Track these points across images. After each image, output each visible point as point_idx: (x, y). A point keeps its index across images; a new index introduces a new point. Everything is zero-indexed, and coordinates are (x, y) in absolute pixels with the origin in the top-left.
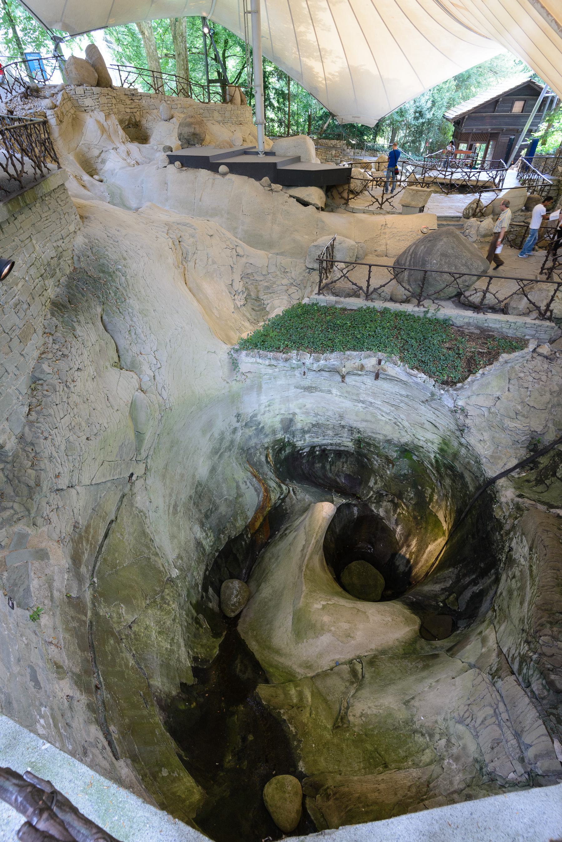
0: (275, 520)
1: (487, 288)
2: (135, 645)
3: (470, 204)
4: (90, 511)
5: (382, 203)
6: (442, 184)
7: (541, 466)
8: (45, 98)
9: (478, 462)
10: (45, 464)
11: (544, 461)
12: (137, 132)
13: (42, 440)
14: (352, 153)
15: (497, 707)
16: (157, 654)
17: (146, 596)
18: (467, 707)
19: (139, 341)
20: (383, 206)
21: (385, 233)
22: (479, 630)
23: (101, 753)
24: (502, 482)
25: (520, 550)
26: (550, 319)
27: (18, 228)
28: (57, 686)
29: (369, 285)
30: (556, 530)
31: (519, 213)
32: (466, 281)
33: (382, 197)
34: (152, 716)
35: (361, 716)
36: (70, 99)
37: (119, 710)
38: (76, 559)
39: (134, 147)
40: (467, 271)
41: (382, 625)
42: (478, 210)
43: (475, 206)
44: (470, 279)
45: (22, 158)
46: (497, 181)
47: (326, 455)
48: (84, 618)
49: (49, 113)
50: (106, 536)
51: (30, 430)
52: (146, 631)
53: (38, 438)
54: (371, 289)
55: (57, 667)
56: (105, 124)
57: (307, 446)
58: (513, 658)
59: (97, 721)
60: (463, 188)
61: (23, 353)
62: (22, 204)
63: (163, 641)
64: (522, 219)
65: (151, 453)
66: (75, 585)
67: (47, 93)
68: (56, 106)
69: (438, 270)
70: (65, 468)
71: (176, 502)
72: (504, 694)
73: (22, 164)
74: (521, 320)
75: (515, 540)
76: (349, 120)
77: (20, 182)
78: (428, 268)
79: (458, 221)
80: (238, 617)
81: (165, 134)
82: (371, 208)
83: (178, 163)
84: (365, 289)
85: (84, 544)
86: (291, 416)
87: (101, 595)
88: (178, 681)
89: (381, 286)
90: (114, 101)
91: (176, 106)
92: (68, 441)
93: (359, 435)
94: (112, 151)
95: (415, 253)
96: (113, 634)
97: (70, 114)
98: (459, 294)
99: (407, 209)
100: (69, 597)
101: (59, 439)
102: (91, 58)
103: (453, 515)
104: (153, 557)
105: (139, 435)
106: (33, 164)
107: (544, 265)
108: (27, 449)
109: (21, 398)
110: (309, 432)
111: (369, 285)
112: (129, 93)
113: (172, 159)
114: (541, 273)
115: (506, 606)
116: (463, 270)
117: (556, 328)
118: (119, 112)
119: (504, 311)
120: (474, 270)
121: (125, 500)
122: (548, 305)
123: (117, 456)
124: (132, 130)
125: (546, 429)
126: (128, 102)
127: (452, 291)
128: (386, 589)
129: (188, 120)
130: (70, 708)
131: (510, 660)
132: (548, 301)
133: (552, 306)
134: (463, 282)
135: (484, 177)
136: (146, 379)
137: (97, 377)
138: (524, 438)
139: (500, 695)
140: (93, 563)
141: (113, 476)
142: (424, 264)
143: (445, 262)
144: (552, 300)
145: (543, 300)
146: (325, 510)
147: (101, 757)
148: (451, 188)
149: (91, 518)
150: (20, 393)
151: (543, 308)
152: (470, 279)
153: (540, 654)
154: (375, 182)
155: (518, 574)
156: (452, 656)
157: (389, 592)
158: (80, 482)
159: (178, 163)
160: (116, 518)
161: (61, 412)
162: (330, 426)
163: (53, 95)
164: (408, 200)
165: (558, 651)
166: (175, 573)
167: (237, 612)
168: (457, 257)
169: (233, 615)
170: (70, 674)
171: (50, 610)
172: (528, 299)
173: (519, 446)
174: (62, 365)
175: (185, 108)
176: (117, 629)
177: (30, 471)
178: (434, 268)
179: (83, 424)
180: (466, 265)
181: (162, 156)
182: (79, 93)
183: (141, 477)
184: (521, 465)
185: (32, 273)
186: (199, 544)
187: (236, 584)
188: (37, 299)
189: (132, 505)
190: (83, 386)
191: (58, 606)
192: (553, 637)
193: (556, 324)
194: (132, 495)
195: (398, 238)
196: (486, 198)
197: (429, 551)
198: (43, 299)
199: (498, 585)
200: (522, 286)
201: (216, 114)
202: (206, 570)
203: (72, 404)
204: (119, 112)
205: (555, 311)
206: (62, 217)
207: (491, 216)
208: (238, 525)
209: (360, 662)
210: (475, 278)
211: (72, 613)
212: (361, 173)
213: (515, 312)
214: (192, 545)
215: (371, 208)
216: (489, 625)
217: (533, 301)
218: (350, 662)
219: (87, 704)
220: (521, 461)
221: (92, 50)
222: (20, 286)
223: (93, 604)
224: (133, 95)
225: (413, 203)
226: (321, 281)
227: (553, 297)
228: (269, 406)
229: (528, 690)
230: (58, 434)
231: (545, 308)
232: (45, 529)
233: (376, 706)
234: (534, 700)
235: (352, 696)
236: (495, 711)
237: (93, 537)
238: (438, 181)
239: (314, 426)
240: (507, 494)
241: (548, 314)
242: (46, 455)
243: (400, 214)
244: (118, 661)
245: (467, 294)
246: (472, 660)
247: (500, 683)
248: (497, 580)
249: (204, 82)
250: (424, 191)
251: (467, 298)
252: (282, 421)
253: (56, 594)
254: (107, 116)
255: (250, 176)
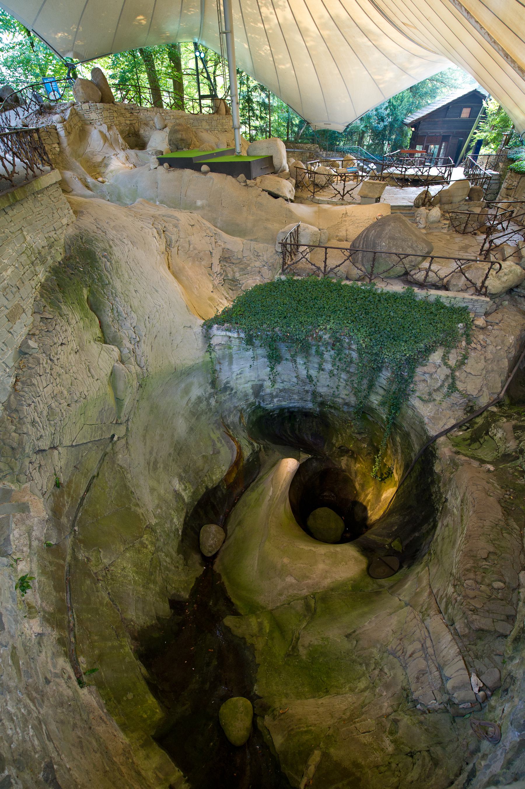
0: (247, 474)
1: (430, 267)
2: (111, 584)
3: (420, 194)
4: (71, 469)
5: (344, 195)
6: (398, 179)
7: (476, 426)
8: (56, 113)
9: (422, 422)
10: (28, 428)
11: (480, 421)
12: (136, 141)
13: (25, 407)
14: (324, 155)
15: (425, 642)
16: (133, 591)
17: (125, 541)
18: (399, 642)
19: (121, 318)
20: (345, 198)
21: (345, 221)
22: (417, 571)
23: (66, 682)
24: (442, 439)
25: (453, 501)
26: (485, 294)
27: (9, 221)
28: (27, 625)
29: (326, 266)
30: (485, 483)
31: (463, 202)
32: (412, 261)
33: (344, 190)
34: (122, 647)
35: (309, 647)
36: (77, 114)
37: (90, 643)
38: (56, 512)
39: (132, 153)
40: (414, 253)
41: (339, 564)
42: (426, 200)
43: (424, 196)
44: (416, 259)
45: (14, 160)
46: (446, 176)
47: (295, 416)
48: (62, 562)
49: (59, 126)
50: (87, 490)
51: (15, 398)
52: (123, 572)
53: (22, 405)
54: (328, 269)
55: (30, 608)
56: (107, 134)
57: (276, 409)
58: (442, 599)
59: (66, 654)
60: (416, 182)
61: (11, 330)
62: (11, 200)
63: (138, 581)
64: (466, 207)
65: (132, 416)
66: (54, 534)
67: (58, 111)
68: (65, 120)
69: (387, 251)
70: (46, 431)
71: (156, 460)
72: (431, 631)
73: (14, 165)
74: (461, 295)
75: (450, 493)
76: (322, 126)
77: (11, 181)
78: (378, 249)
79: (409, 210)
80: (215, 556)
81: (158, 141)
82: (334, 200)
83: (166, 165)
84: (323, 269)
85: (65, 498)
86: (260, 382)
87: (81, 541)
88: (153, 613)
89: (337, 267)
90: (115, 114)
91: (169, 118)
92: (50, 407)
93: (321, 399)
94: (113, 157)
95: (367, 236)
96: (89, 575)
97: (77, 127)
98: (407, 273)
99: (365, 199)
100: (49, 545)
101: (42, 406)
102: (96, 80)
103: (402, 469)
104: (133, 508)
105: (119, 401)
106: (25, 166)
107: (483, 247)
108: (13, 415)
109: (8, 370)
110: (277, 396)
111: (326, 266)
112: (128, 107)
113: (161, 161)
114: (480, 254)
115: (439, 551)
116: (409, 251)
117: (492, 302)
118: (120, 124)
119: (446, 287)
120: (419, 251)
121: (107, 458)
122: (483, 282)
123: (97, 420)
124: (133, 139)
125: (481, 393)
126: (128, 115)
127: (399, 269)
128: (345, 532)
129: (176, 127)
130: (39, 643)
131: (438, 600)
132: (484, 278)
133: (487, 283)
134: (409, 262)
135: (434, 172)
136: (126, 351)
137: (80, 351)
138: (461, 401)
139: (428, 631)
140: (74, 514)
141: (94, 437)
142: (374, 246)
143: (393, 245)
144: (487, 277)
145: (479, 278)
146: (290, 465)
147: (65, 686)
148: (405, 182)
149: (73, 474)
150: (7, 366)
151: (479, 284)
152: (416, 259)
153: (464, 597)
154: (339, 178)
155: (451, 523)
156: (392, 594)
157: (348, 535)
158: (61, 443)
159: (166, 165)
160: (98, 474)
161: (44, 382)
162: (296, 391)
163: (62, 112)
164: (366, 192)
165: (480, 593)
166: (154, 521)
167: (214, 553)
168: (403, 240)
169: (210, 555)
170: (42, 613)
171: (28, 556)
172: (466, 277)
173: (457, 408)
174: (48, 341)
175: (177, 119)
176: (95, 571)
177: (14, 434)
178: (383, 250)
179: (65, 392)
180: (411, 247)
181: (153, 161)
182: (85, 108)
183: (123, 438)
184: (459, 426)
185: (22, 261)
186: (177, 495)
187: (213, 528)
188: (27, 282)
189: (114, 462)
190: (66, 359)
191: (35, 554)
192: (476, 582)
193: (491, 299)
194: (114, 454)
195: (356, 225)
196: (434, 190)
197: (380, 499)
198: (33, 283)
199: (435, 531)
200: (460, 264)
201: (204, 123)
202: (186, 516)
203: (55, 375)
204: (120, 124)
205: (490, 287)
206: (55, 212)
207: (439, 205)
208: (214, 478)
209: (314, 598)
210: (420, 258)
211: (50, 558)
212: (326, 170)
213: (455, 289)
214: (170, 497)
215: (334, 200)
216: (424, 567)
217: (470, 278)
218: (306, 598)
219: (58, 639)
220: (459, 421)
221: (96, 72)
222: (9, 272)
223: (73, 549)
224: (132, 109)
225: (370, 195)
226: (284, 263)
227: (487, 275)
228: (240, 374)
229: (452, 628)
230: (40, 402)
231: (481, 285)
232: (28, 485)
233: (323, 638)
234: (456, 637)
235: (304, 628)
236: (423, 646)
237: (74, 491)
238: (394, 176)
239: (281, 391)
240: (444, 449)
241: (484, 290)
242: (29, 420)
243: (359, 204)
244: (93, 599)
245: (412, 273)
246: (407, 599)
247: (428, 621)
248: (435, 527)
249: (197, 96)
250: (379, 184)
251: (412, 276)
252: (253, 387)
253: (35, 543)
254: (109, 128)
255: (228, 174)
